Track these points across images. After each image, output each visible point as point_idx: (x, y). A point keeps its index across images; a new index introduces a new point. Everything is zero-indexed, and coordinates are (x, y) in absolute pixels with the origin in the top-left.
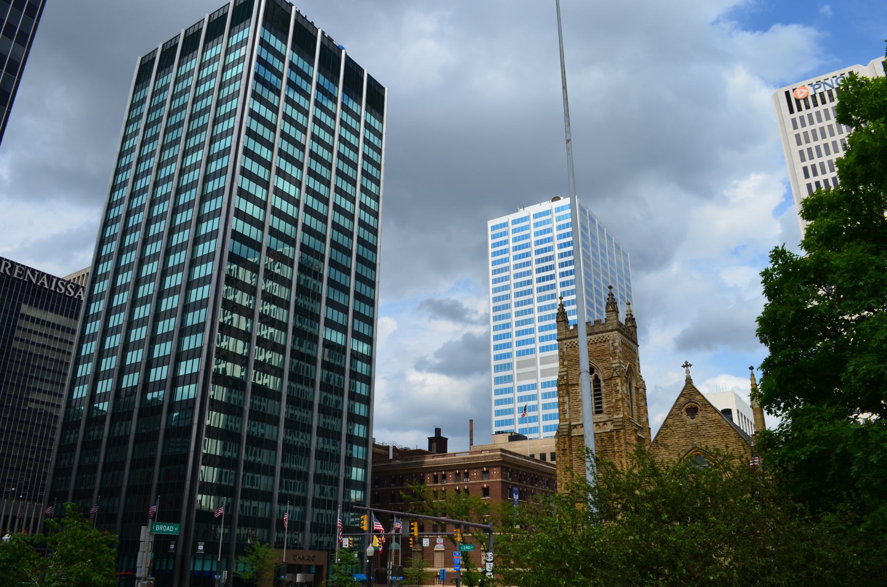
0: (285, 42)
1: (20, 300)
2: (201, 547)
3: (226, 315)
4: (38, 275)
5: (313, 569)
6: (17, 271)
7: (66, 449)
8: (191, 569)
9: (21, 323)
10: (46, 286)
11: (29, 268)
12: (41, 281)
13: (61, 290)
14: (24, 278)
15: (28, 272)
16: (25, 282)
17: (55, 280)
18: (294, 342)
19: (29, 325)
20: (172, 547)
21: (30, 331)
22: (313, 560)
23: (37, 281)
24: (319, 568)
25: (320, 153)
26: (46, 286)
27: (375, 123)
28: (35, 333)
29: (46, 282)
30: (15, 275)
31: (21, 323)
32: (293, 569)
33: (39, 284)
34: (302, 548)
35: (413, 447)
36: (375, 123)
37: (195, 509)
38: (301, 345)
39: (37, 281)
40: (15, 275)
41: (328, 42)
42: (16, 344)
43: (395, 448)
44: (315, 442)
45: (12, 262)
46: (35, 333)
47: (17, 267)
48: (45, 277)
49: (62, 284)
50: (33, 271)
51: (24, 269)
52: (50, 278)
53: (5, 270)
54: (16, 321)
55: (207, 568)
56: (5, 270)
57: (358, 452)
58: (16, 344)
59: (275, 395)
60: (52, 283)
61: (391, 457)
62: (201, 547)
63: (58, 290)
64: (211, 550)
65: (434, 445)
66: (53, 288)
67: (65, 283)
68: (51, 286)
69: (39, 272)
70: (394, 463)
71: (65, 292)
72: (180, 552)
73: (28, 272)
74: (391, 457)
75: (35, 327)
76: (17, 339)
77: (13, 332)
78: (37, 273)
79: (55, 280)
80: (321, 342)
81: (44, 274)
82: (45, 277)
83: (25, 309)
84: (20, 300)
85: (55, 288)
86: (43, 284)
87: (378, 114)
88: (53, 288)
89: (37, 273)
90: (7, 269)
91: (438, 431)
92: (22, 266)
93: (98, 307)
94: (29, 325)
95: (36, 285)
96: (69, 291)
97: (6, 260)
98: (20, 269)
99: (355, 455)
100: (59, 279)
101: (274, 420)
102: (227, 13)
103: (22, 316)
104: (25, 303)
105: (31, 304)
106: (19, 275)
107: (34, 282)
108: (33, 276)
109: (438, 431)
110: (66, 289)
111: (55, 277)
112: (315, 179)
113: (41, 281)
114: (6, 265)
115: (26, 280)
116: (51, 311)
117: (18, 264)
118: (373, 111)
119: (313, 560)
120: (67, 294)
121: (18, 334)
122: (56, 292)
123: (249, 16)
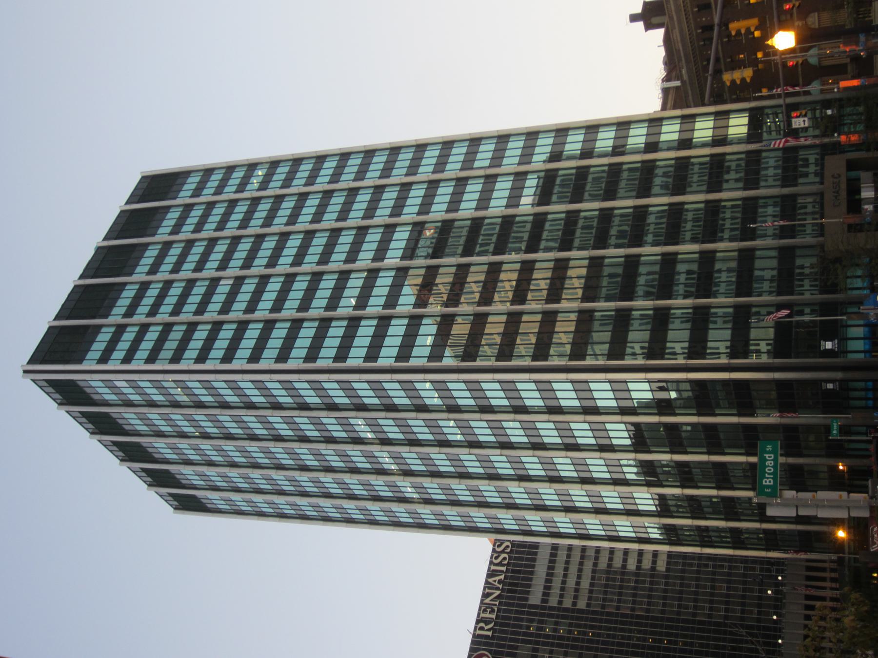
0: (98, 329)
1: (524, 606)
2: (829, 345)
3: (485, 352)
4: (489, 588)
5: (853, 174)
6: (487, 615)
7: (704, 537)
8: (862, 356)
9: (553, 601)
10: (502, 577)
11: (482, 602)
12: (496, 584)
13: (505, 559)
14: (495, 605)
15: (487, 601)
16: (500, 604)
17: (493, 568)
18: (453, 255)
19: (556, 591)
20: (830, 386)
21: (562, 589)
22: (839, 176)
23: (498, 589)
24: (851, 165)
25: (294, 251)
26: (502, 577)
27: (192, 182)
28: (564, 582)
29: (497, 578)
30: (494, 616)
31: (553, 601)
32: (854, 204)
33: (501, 586)
34: (822, 194)
35: (662, 53)
36: (192, 182)
37: (771, 361)
38: (520, 240)
39: (498, 589)
40: (494, 616)
41: (92, 270)
42: (582, 604)
43: (667, 79)
44: (659, 201)
45: (478, 622)
46: (564, 582)
47: (482, 615)
48: (491, 580)
49: (496, 558)
50: (485, 595)
51: (484, 607)
52: (491, 574)
53: (489, 630)
54: (552, 608)
55: (859, 332)
56: (489, 630)
57: (670, 132)
58: (582, 604)
59: (595, 264)
60: (497, 571)
61: (677, 83)
62: (829, 345)
63: (506, 562)
64: (833, 331)
65: (655, 20)
66: (504, 569)
67: (495, 555)
68: (502, 571)
69: (485, 588)
70: (685, 77)
71: (507, 553)
72: (839, 375)
73: (487, 601)
74: (677, 83)
75: (557, 583)
76: (574, 604)
77: (566, 610)
78: (487, 590)
79: (493, 568)
80: (511, 211)
81: (487, 582)
82: (491, 580)
83: (535, 598)
84: (524, 606)
85: (504, 565)
86: (500, 582)
87: (179, 181)
88: (504, 569)
89: (487, 590)
90: (486, 627)
91: (634, 18)
92: (480, 609)
93: (507, 518)
94: (556, 591)
95: (503, 590)
96: (505, 549)
97: (475, 629)
98: (485, 611)
99: (675, 136)
100: (491, 563)
101: (632, 263)
102: (80, 412)
103: (544, 601)
104: (527, 599)
105: (528, 593)
106: (492, 611)
107: (498, 592)
108: (491, 594)
109: (634, 18)
110: (503, 552)
111: (489, 568)
112: (255, 258)
113: (496, 584)
114: (482, 629)
115: (497, 603)
116: (533, 566)
117: (479, 614)
118: (175, 188)
119: (839, 176)
120: (508, 550)
121: (567, 603)
122: (508, 564)
123: (73, 383)
